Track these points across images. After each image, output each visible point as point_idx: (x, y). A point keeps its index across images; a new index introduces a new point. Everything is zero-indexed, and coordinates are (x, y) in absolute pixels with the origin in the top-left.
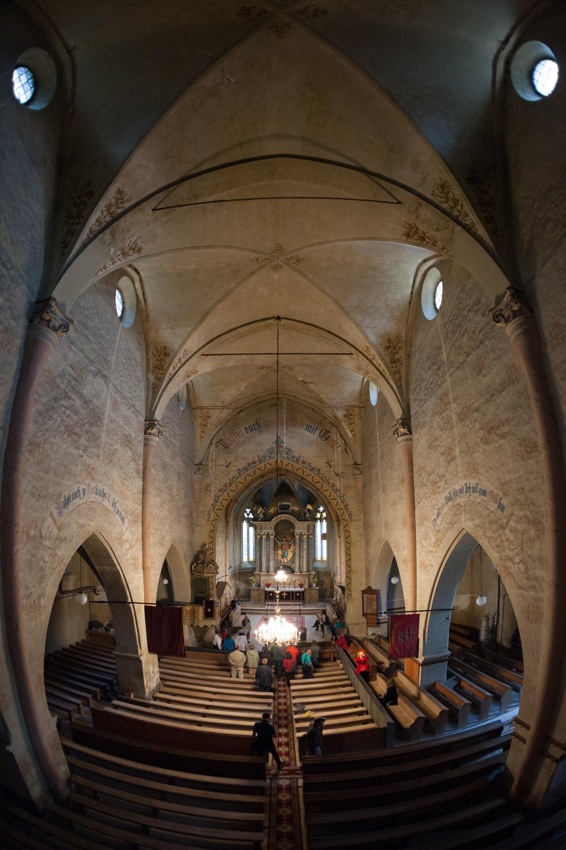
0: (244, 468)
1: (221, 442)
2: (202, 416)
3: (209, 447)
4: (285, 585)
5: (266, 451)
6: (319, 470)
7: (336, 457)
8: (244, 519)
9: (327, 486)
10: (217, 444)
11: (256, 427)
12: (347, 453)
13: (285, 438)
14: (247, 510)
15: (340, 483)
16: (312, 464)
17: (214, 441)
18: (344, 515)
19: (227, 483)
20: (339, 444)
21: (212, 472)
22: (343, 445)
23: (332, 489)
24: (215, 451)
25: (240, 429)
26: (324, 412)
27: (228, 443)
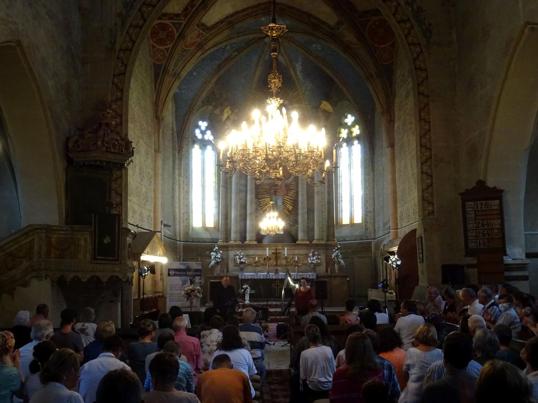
4: (279, 268)
8: (195, 140)
14: (201, 123)
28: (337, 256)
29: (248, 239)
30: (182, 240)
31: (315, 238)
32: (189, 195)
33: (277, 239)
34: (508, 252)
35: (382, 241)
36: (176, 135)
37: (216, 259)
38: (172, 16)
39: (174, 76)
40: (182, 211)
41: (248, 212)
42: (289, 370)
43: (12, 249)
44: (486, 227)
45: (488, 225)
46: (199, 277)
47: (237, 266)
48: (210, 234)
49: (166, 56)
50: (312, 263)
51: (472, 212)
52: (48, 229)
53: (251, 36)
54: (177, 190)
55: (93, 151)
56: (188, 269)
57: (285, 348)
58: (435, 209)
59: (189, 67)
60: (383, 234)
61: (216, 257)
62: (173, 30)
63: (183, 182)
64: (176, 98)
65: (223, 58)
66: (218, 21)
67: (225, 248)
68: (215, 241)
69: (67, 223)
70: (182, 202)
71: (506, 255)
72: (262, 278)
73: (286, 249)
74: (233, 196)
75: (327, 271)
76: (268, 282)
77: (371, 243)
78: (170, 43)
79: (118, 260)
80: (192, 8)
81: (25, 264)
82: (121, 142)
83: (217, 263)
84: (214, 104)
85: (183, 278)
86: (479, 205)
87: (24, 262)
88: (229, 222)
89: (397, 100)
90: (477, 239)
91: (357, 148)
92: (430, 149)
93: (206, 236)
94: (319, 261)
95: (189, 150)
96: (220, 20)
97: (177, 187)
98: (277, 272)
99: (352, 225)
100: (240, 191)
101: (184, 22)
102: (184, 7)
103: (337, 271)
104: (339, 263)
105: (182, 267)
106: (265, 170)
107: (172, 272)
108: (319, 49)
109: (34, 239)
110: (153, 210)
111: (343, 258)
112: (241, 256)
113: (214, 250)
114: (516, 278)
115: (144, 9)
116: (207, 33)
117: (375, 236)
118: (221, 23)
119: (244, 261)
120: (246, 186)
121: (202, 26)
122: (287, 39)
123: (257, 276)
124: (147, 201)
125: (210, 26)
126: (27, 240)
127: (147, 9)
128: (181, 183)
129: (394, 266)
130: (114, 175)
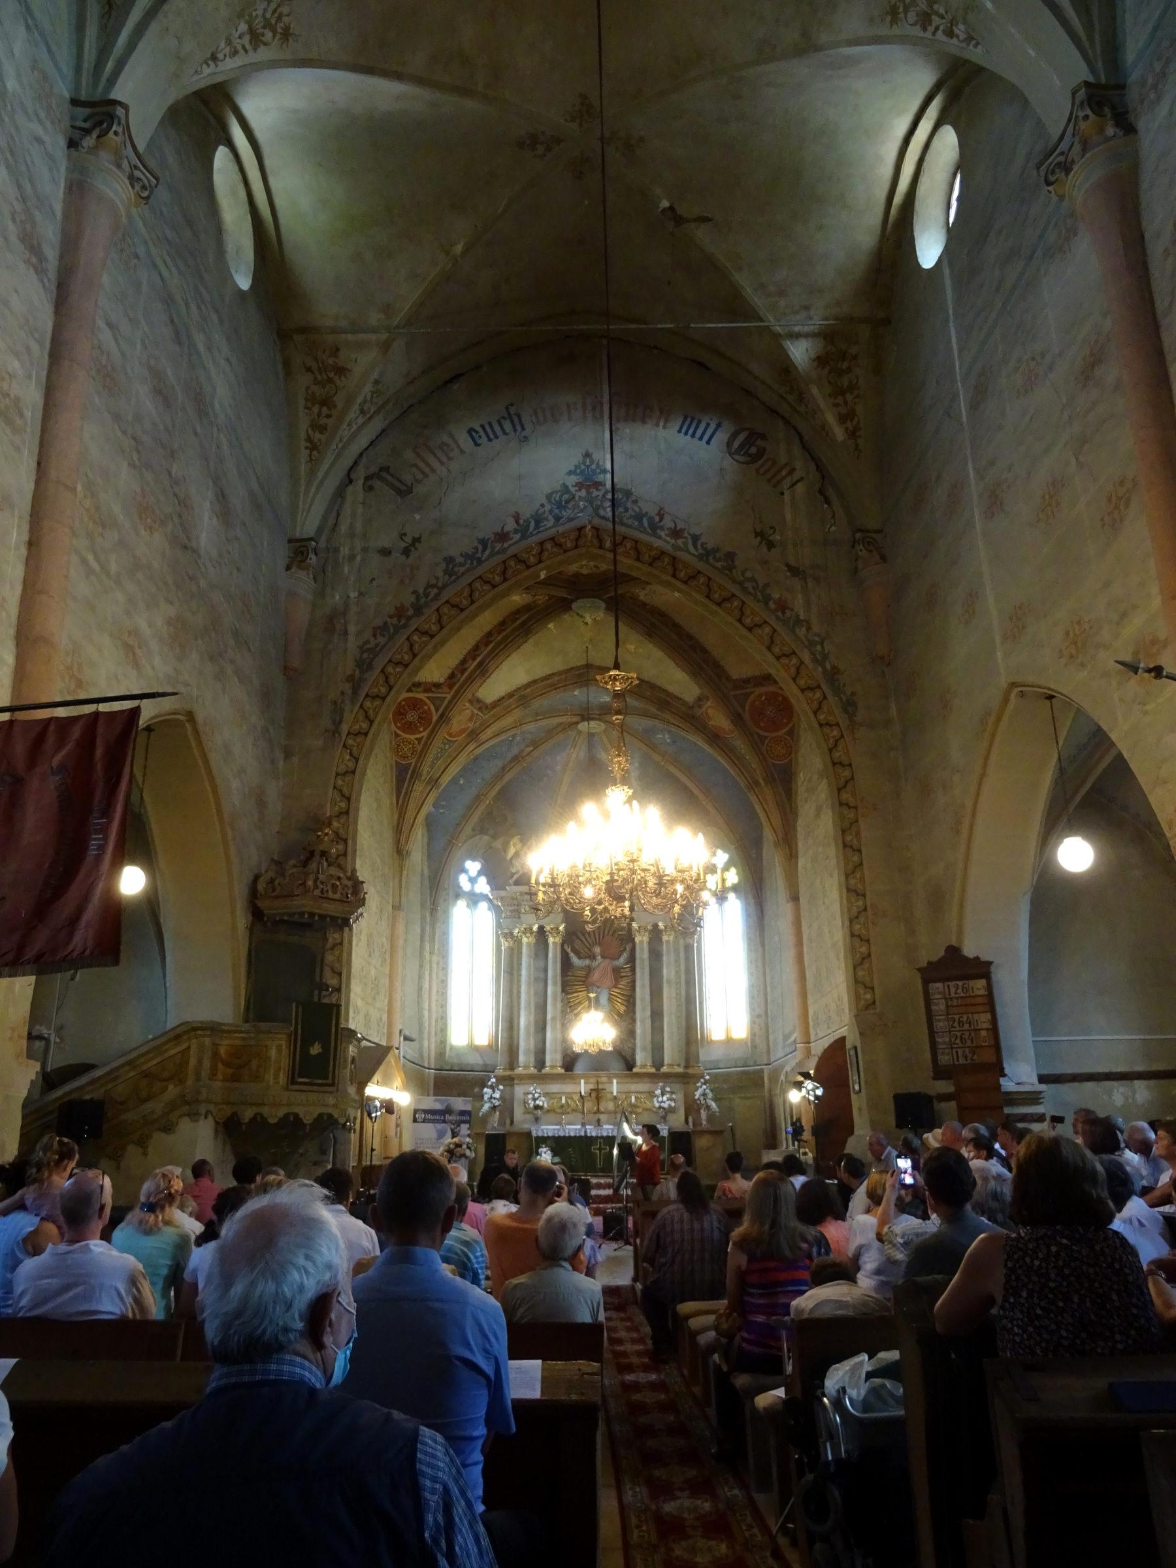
0: (466, 556)
1: (384, 474)
2: (314, 365)
3: (340, 493)
4: (603, 1117)
5: (545, 501)
6: (730, 556)
7: (788, 517)
8: (458, 894)
10: (369, 483)
11: (507, 426)
12: (827, 501)
16: (703, 539)
17: (360, 474)
18: (825, 708)
20: (797, 475)
23: (778, 618)
24: (363, 503)
25: (452, 436)
27: (408, 478)
28: (704, 1095)
29: (548, 1063)
30: (433, 1067)
31: (666, 1061)
32: (446, 987)
33: (598, 1061)
34: (1008, 1070)
35: (783, 1067)
36: (427, 882)
37: (494, 1101)
38: (431, 687)
39: (428, 783)
40: (434, 1016)
41: (549, 1017)
42: (633, 1288)
43: (150, 1064)
44: (966, 1026)
45: (970, 1023)
46: (468, 1126)
47: (529, 1113)
48: (482, 1057)
50: (660, 1107)
51: (940, 1001)
52: (213, 1029)
53: (555, 721)
54: (427, 978)
55: (298, 895)
56: (448, 1111)
57: (619, 1253)
58: (877, 997)
59: (454, 769)
60: (783, 1054)
61: (491, 1097)
62: (429, 708)
63: (438, 964)
64: (429, 823)
65: (510, 756)
67: (508, 1081)
68: (489, 1069)
69: (246, 1021)
70: (434, 998)
71: (1004, 1075)
72: (572, 1134)
73: (615, 1081)
74: (523, 988)
75: (687, 1121)
76: (585, 1142)
77: (762, 1071)
79: (333, 1085)
80: (462, 673)
81: (172, 1091)
82: (346, 882)
83: (494, 1108)
84: (491, 832)
85: (440, 1126)
86: (953, 990)
87: (171, 1087)
88: (515, 1033)
89: (801, 822)
90: (952, 1048)
91: (735, 906)
92: (864, 895)
93: (474, 1060)
94: (673, 1104)
95: (448, 909)
97: (427, 973)
98: (599, 1123)
99: (729, 1041)
100: (536, 979)
101: (449, 696)
102: (450, 671)
103: (704, 1123)
104: (708, 1107)
105: (438, 1106)
106: (602, 906)
107: (420, 1116)
108: (668, 741)
109: (189, 1048)
110: (386, 1008)
111: (715, 1099)
112: (537, 1095)
113: (490, 1083)
114: (1025, 1118)
115: (390, 669)
116: (485, 715)
117: (769, 1059)
119: (541, 1104)
120: (546, 970)
121: (477, 702)
123: (564, 1130)
124: (378, 993)
126: (179, 1049)
128: (434, 966)
129: (812, 1098)
130: (330, 940)
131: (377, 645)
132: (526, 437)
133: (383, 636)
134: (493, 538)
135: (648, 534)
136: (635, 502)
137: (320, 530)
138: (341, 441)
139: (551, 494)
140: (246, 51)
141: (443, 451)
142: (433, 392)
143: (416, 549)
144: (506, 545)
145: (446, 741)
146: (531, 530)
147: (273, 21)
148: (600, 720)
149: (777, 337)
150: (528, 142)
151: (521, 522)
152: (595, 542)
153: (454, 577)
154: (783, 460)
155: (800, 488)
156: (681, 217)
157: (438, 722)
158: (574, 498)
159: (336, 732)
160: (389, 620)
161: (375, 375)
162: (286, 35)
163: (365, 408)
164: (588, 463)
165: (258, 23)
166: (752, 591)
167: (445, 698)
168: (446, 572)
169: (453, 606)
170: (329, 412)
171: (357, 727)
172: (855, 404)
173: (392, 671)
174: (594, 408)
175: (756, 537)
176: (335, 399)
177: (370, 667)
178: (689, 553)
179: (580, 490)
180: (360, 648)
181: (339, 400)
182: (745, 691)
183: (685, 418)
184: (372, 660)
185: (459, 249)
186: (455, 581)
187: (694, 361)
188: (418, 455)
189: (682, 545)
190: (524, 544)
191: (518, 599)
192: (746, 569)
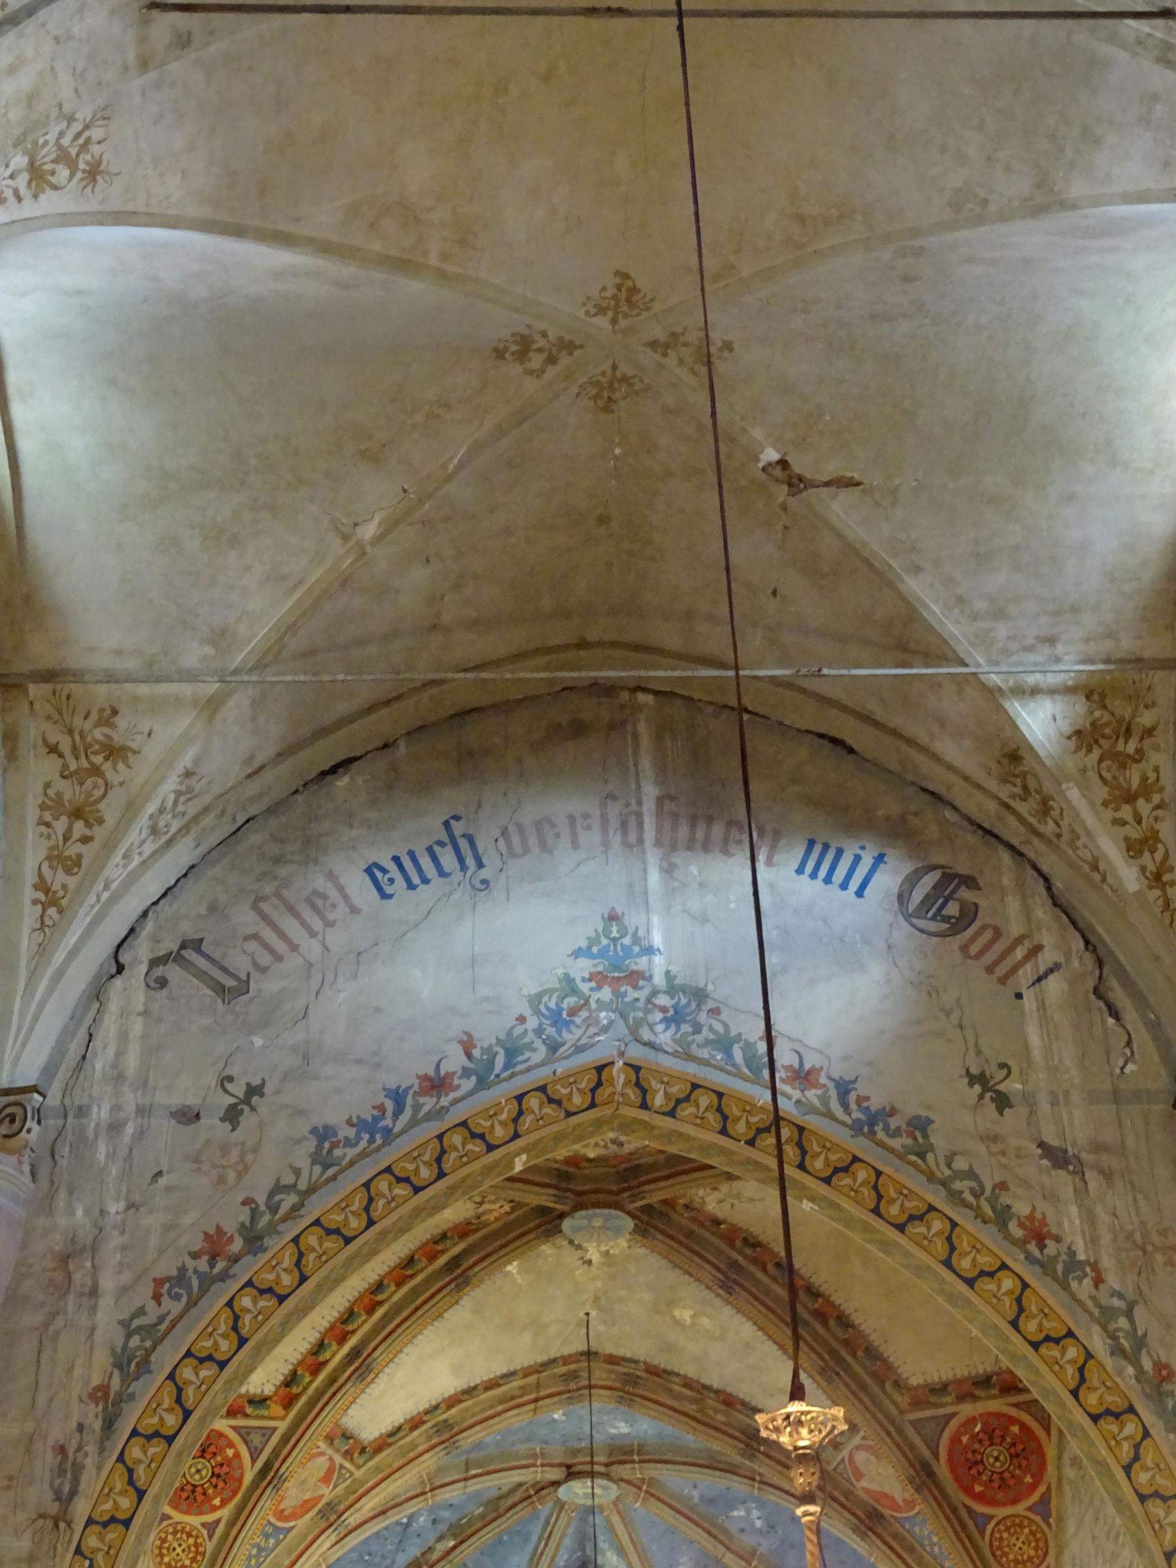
0: (359, 1124)
1: (189, 954)
2: (65, 746)
3: (97, 993)
5: (527, 1012)
6: (920, 1125)
7: (1035, 1040)
9: (988, 1235)
10: (159, 971)
11: (448, 859)
12: (1115, 1013)
13: (655, 919)
15: (1090, 1218)
16: (861, 1089)
17: (140, 953)
18: (1148, 1458)
19: (230, 1227)
20: (1047, 958)
21: (112, 1156)
22: (1080, 962)
23: (1029, 1257)
24: (145, 1013)
25: (331, 876)
26: (922, 749)
27: (240, 963)
49: (204, 1554)
53: (515, 1477)
62: (237, 1455)
66: (402, 1421)
78: (224, 1503)
96: (409, 1417)
101: (282, 1426)
108: (758, 1524)
116: (358, 1467)
118: (414, 1427)
122: (640, 1488)
125: (371, 1438)
127: (197, 1374)
131: (161, 1319)
132: (484, 882)
133: (177, 1297)
134: (416, 1088)
135: (745, 1079)
136: (715, 1012)
137: (49, 1070)
138: (106, 887)
139: (540, 995)
140: (19, 199)
141: (313, 906)
142: (296, 792)
143: (253, 1109)
144: (445, 1101)
145: (269, 1530)
146: (497, 1070)
147: (73, 152)
148: (607, 1476)
149: (992, 693)
150: (514, 348)
151: (476, 1053)
152: (633, 1095)
153: (331, 1172)
154: (1015, 929)
155: (1054, 984)
156: (801, 479)
157: (255, 1484)
158: (587, 1002)
159: (61, 1519)
160: (190, 1263)
161: (187, 760)
162: (93, 173)
163: (162, 823)
164: (615, 934)
165: (47, 154)
166: (970, 1198)
167: (274, 1429)
168: (316, 1158)
169: (329, 1232)
170: (88, 832)
171: (109, 1506)
172: (1156, 819)
173: (192, 1377)
174: (624, 825)
175: (971, 1085)
176: (102, 806)
177: (144, 1366)
178: (834, 1118)
179: (599, 987)
180: (125, 1324)
181: (110, 810)
182: (942, 1411)
183: (811, 843)
184: (149, 1352)
185: (369, 531)
186: (334, 1178)
187: (822, 736)
188: (265, 917)
189: (816, 1102)
190: (485, 1098)
191: (456, 1212)
192: (954, 1154)
